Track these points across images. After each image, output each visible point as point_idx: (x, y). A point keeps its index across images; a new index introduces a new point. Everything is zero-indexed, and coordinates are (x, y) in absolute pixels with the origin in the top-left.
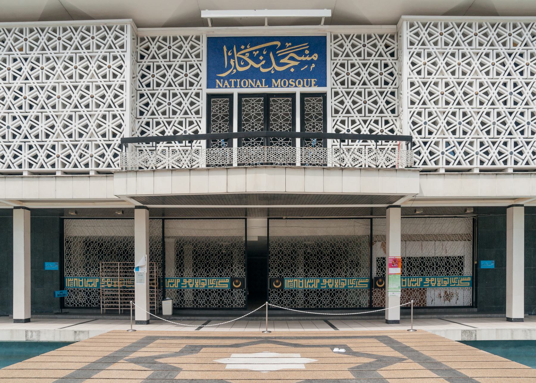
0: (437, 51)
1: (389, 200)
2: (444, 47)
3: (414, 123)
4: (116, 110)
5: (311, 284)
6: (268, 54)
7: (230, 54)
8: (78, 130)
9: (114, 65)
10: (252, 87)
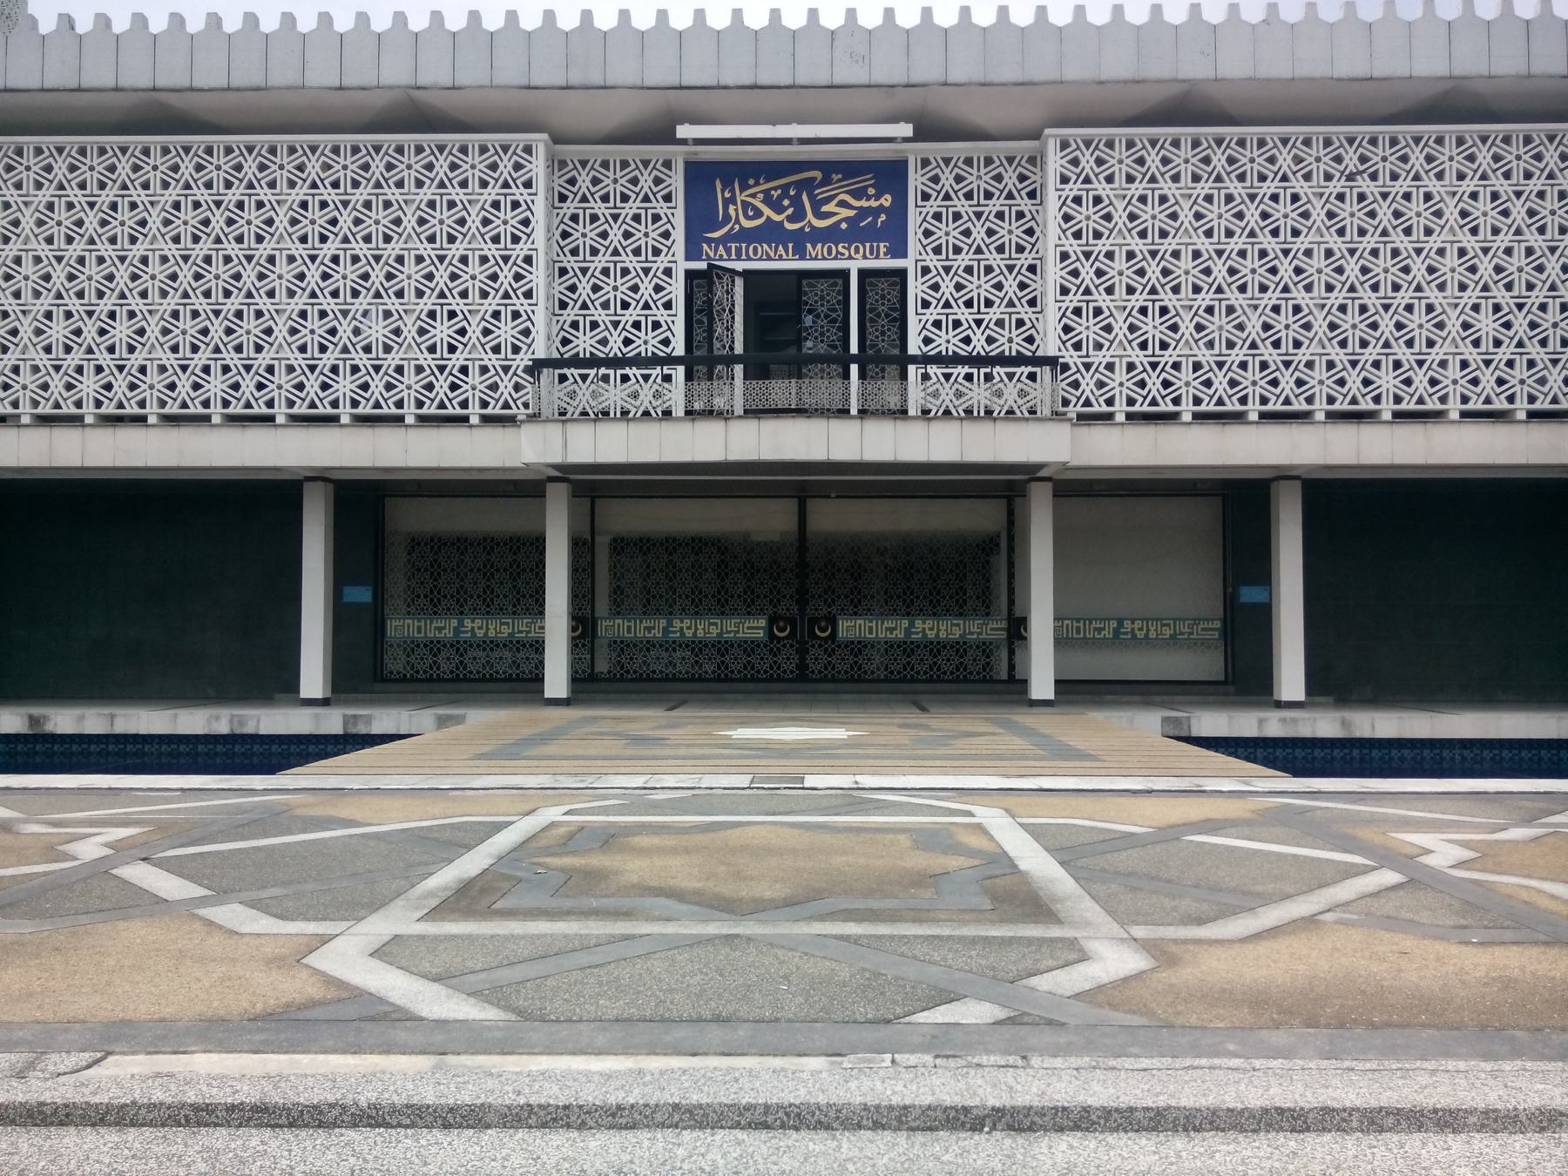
0: (1111, 193)
1: (1031, 472)
2: (1124, 185)
4: (520, 304)
6: (799, 195)
7: (727, 195)
8: (125, 339)
9: (512, 217)
10: (769, 259)
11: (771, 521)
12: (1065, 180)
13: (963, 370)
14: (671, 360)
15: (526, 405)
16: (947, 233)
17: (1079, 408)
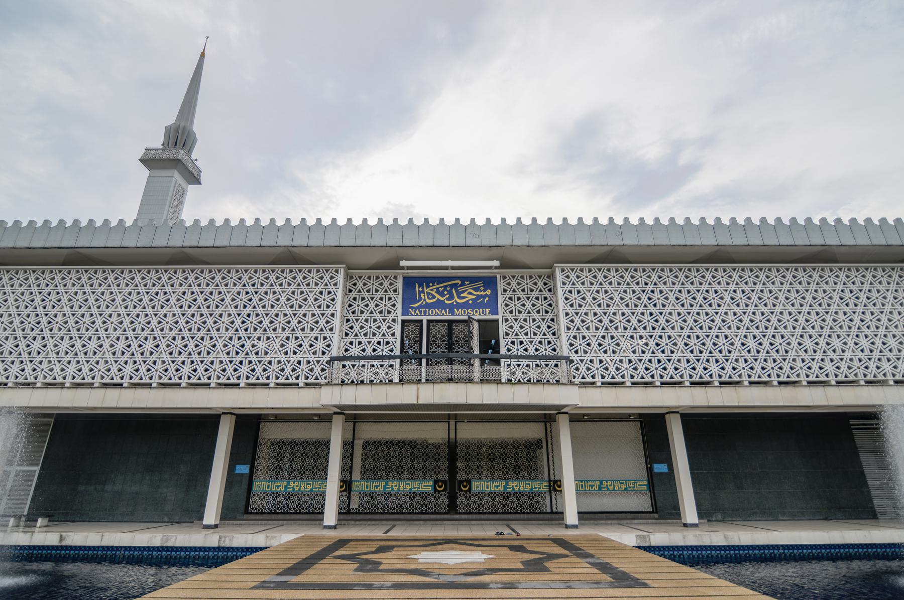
1: (559, 409)
3: (571, 345)
4: (327, 333)
5: (497, 487)
6: (451, 290)
11: (436, 433)
12: (564, 284)
13: (554, 362)
14: (394, 357)
15: (325, 378)
16: (515, 305)
17: (580, 380)
